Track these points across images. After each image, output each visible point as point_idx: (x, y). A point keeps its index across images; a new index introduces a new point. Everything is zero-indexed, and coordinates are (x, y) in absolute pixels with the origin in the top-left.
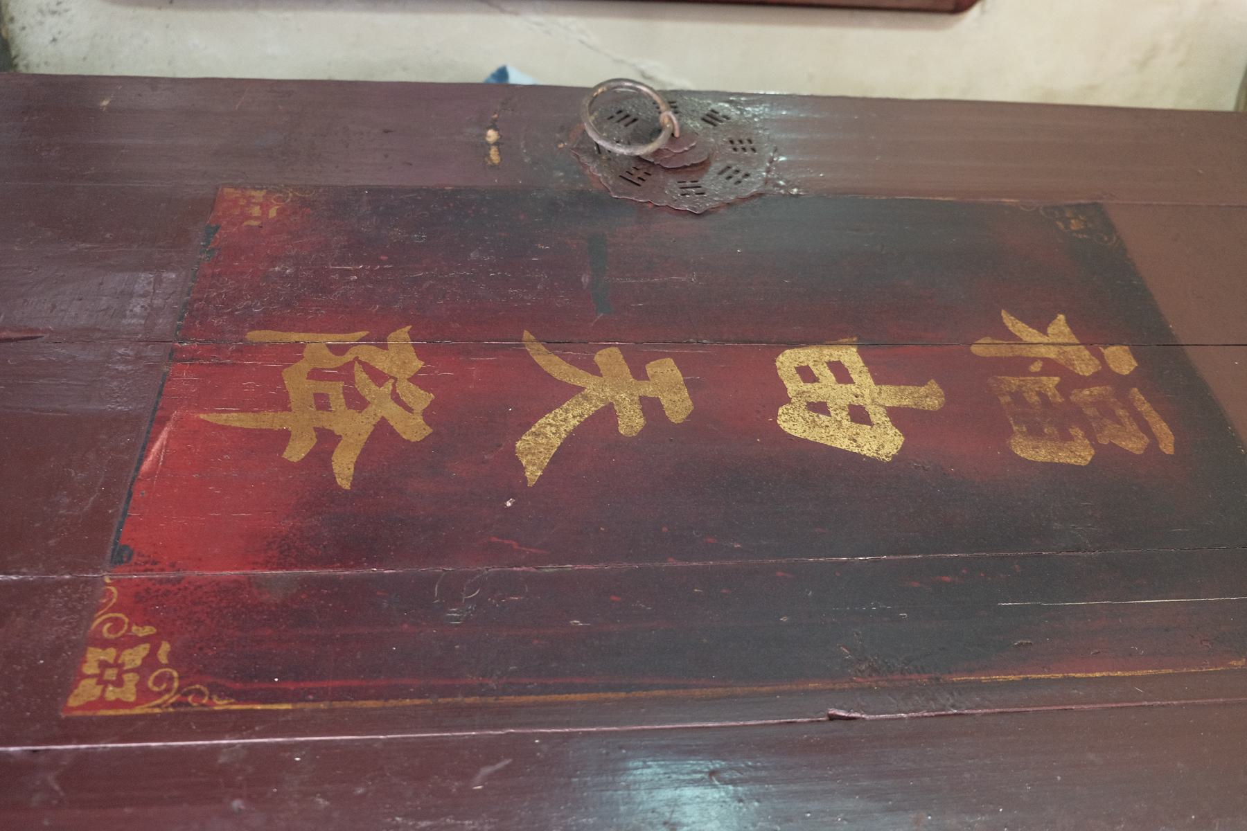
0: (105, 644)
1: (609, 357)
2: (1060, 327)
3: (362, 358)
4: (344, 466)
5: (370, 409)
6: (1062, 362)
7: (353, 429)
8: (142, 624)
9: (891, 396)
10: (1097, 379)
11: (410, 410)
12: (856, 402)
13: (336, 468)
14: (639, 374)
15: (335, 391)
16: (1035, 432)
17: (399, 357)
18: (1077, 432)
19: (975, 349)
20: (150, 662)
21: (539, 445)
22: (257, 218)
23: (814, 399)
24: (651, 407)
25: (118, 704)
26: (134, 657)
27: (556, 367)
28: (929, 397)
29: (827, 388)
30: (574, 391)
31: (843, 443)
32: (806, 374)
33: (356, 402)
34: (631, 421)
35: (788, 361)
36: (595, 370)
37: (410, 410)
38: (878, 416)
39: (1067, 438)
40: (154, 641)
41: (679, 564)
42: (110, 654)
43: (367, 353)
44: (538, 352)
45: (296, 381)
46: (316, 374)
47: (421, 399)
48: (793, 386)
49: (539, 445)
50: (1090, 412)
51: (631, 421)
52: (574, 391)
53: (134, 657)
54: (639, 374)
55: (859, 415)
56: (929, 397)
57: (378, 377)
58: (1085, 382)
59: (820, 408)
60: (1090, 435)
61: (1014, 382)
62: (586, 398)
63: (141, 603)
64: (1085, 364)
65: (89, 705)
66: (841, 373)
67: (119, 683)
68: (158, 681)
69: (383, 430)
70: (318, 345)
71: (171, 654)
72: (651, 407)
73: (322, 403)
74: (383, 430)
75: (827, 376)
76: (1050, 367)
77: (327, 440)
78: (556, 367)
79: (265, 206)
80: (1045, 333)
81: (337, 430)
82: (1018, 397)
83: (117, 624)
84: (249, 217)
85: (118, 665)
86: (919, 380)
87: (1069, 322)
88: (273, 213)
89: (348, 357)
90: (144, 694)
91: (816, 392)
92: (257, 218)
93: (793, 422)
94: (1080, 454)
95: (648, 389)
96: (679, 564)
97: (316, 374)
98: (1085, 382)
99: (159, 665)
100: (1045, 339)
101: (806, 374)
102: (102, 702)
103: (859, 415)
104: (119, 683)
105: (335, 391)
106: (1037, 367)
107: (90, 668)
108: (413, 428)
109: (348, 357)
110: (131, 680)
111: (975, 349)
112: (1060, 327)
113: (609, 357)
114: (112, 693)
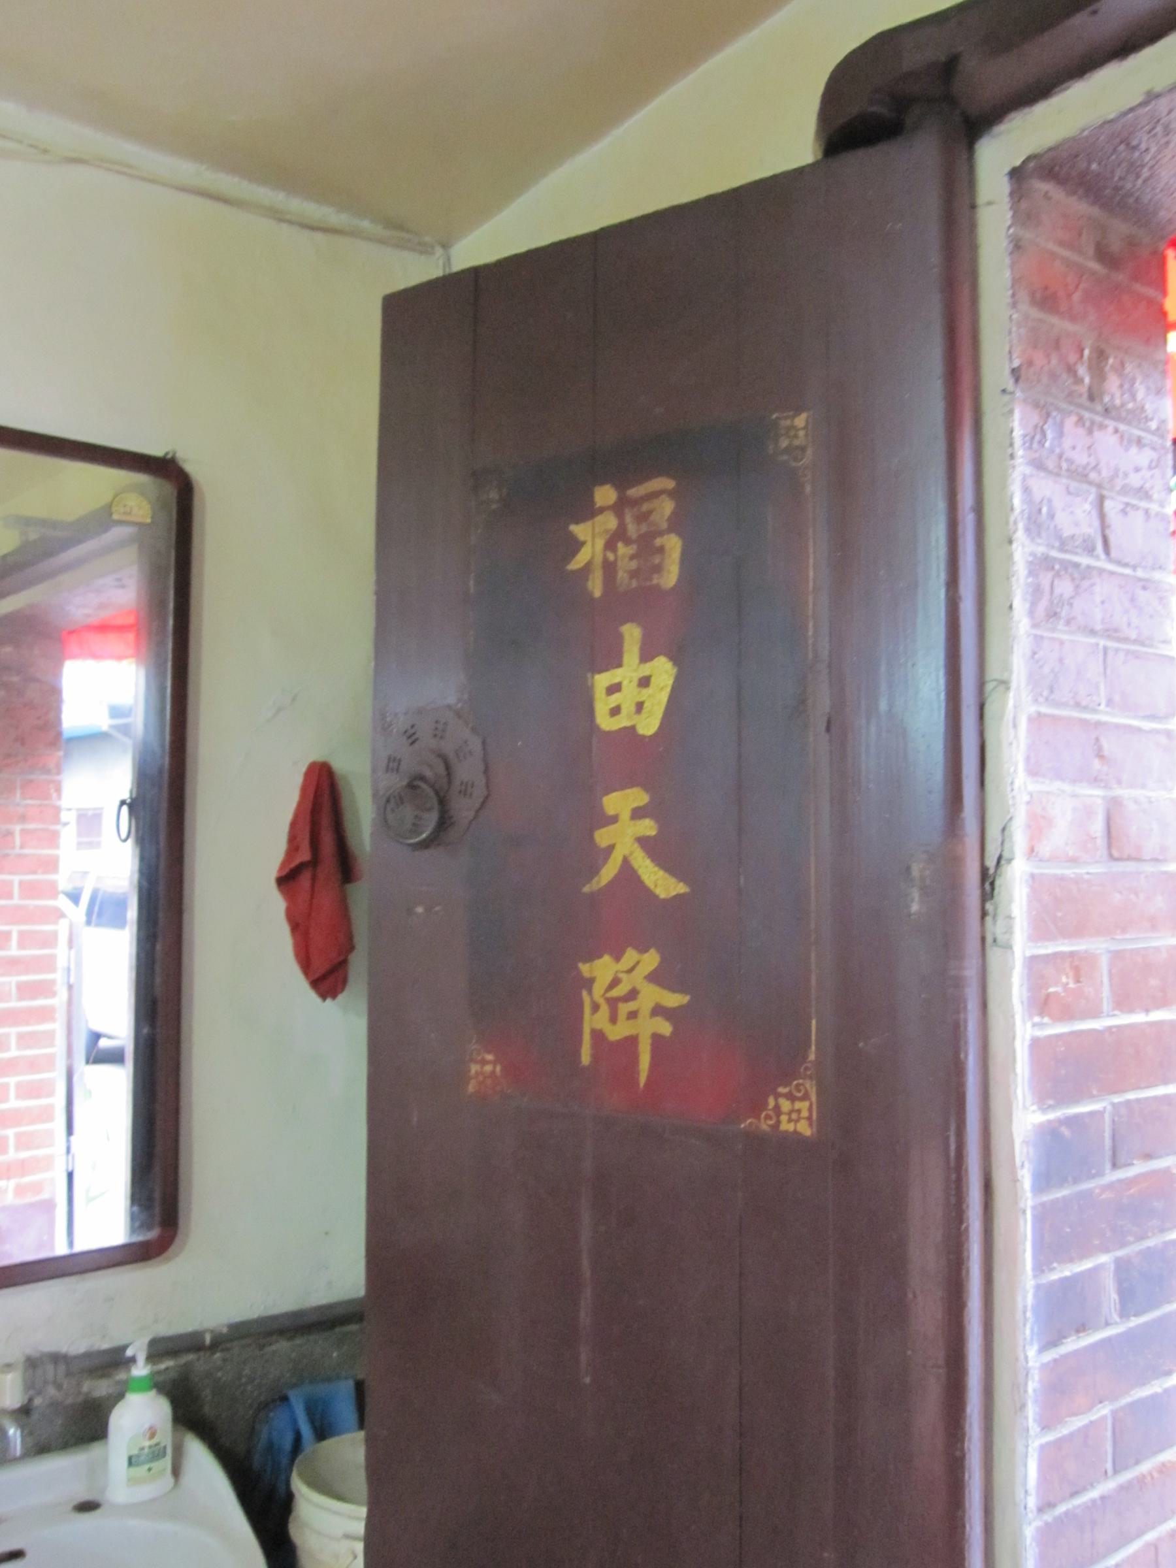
0: (778, 1122)
1: (603, 837)
2: (580, 530)
3: (602, 992)
4: (674, 1000)
5: (639, 987)
6: (608, 536)
7: (652, 995)
8: (766, 1104)
9: (631, 654)
10: (620, 516)
11: (638, 963)
12: (635, 682)
13: (676, 1004)
14: (614, 819)
15: (624, 1008)
16: (658, 569)
17: (602, 970)
18: (658, 542)
19: (597, 593)
20: (791, 1097)
21: (662, 884)
22: (495, 1067)
23: (633, 709)
24: (638, 814)
25: (810, 1110)
26: (785, 1105)
27: (609, 872)
28: (632, 634)
29: (627, 698)
30: (626, 862)
31: (664, 697)
32: (615, 711)
33: (633, 995)
34: (648, 827)
35: (605, 722)
36: (611, 848)
37: (638, 963)
38: (646, 669)
39: (661, 550)
40: (777, 1096)
41: (813, 1048)
42: (784, 1118)
43: (598, 989)
44: (599, 882)
45: (616, 1033)
46: (613, 1019)
47: (631, 956)
48: (621, 722)
49: (662, 884)
50: (644, 528)
51: (648, 827)
52: (626, 862)
53: (785, 1105)
54: (614, 819)
55: (645, 682)
56: (632, 634)
57: (615, 982)
58: (622, 526)
59: (640, 707)
60: (661, 533)
61: (622, 575)
62: (631, 853)
63: (757, 1107)
64: (609, 522)
65: (811, 1125)
66: (614, 689)
67: (799, 1111)
68: (799, 1091)
69: (654, 978)
70: (594, 1021)
71: (785, 1086)
72: (638, 814)
73: (633, 1015)
74: (654, 978)
75: (615, 699)
76: (610, 545)
77: (658, 1011)
78: (609, 872)
79: (484, 1062)
80: (583, 544)
81: (651, 1005)
82: (634, 574)
83: (768, 1117)
84: (493, 1072)
85: (790, 1113)
86: (620, 638)
87: (577, 522)
88: (490, 1057)
89: (602, 1001)
90: (806, 1097)
91: (628, 707)
92: (495, 1067)
93: (649, 725)
94: (673, 544)
95: (625, 815)
96: (813, 1048)
97: (613, 1019)
98: (622, 526)
99: (790, 1092)
100: (589, 544)
101: (615, 711)
102: (809, 1118)
103: (645, 682)
104: (799, 1111)
105: (624, 1008)
106: (611, 557)
107: (790, 1127)
108: (651, 960)
109: (602, 1001)
110: (798, 1105)
111: (597, 593)
112: (580, 530)
113: (603, 837)
114: (805, 1114)
